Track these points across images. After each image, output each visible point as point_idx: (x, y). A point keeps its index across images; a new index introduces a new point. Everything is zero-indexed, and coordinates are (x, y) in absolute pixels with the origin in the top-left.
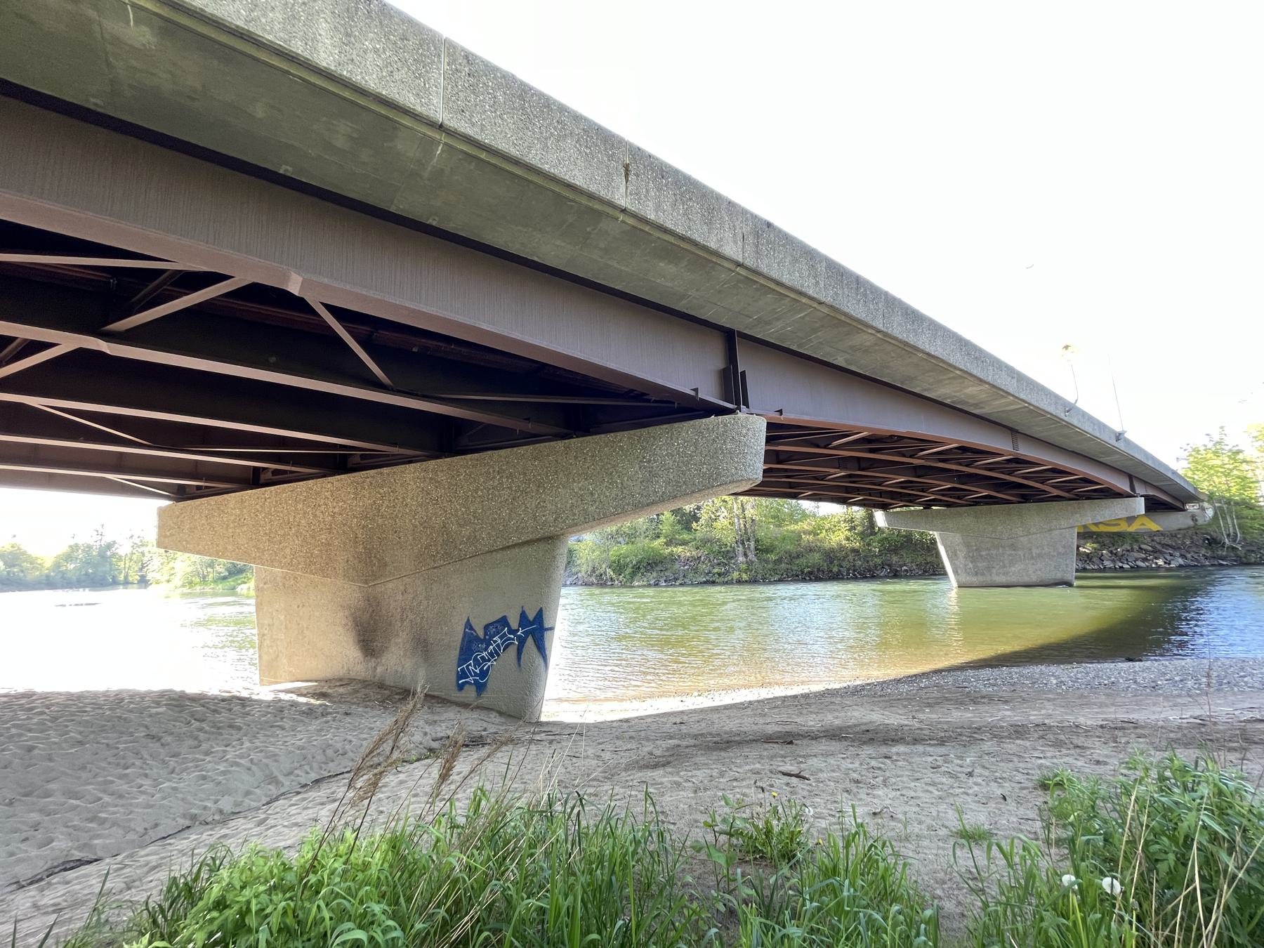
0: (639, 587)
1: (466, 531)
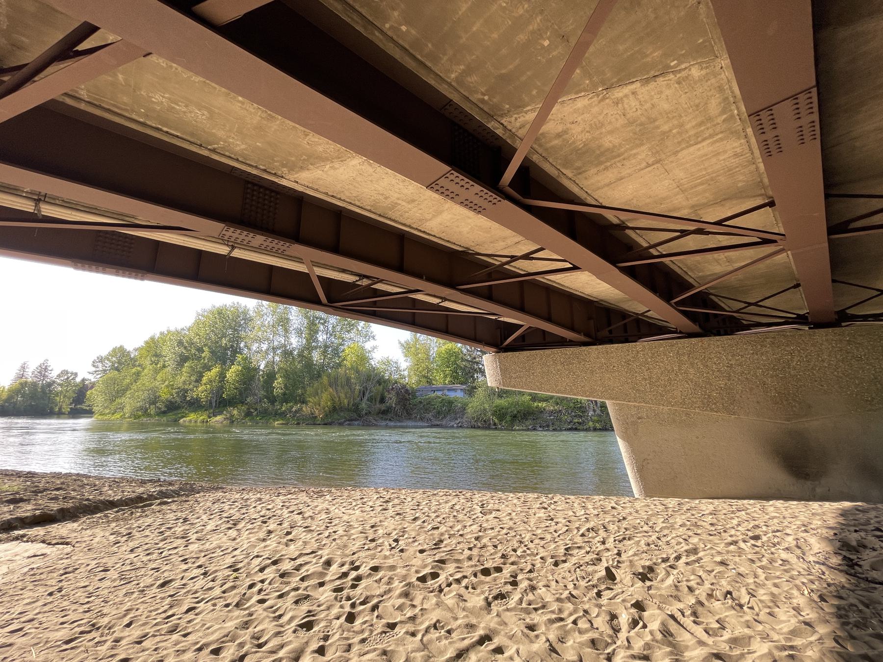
0: (519, 430)
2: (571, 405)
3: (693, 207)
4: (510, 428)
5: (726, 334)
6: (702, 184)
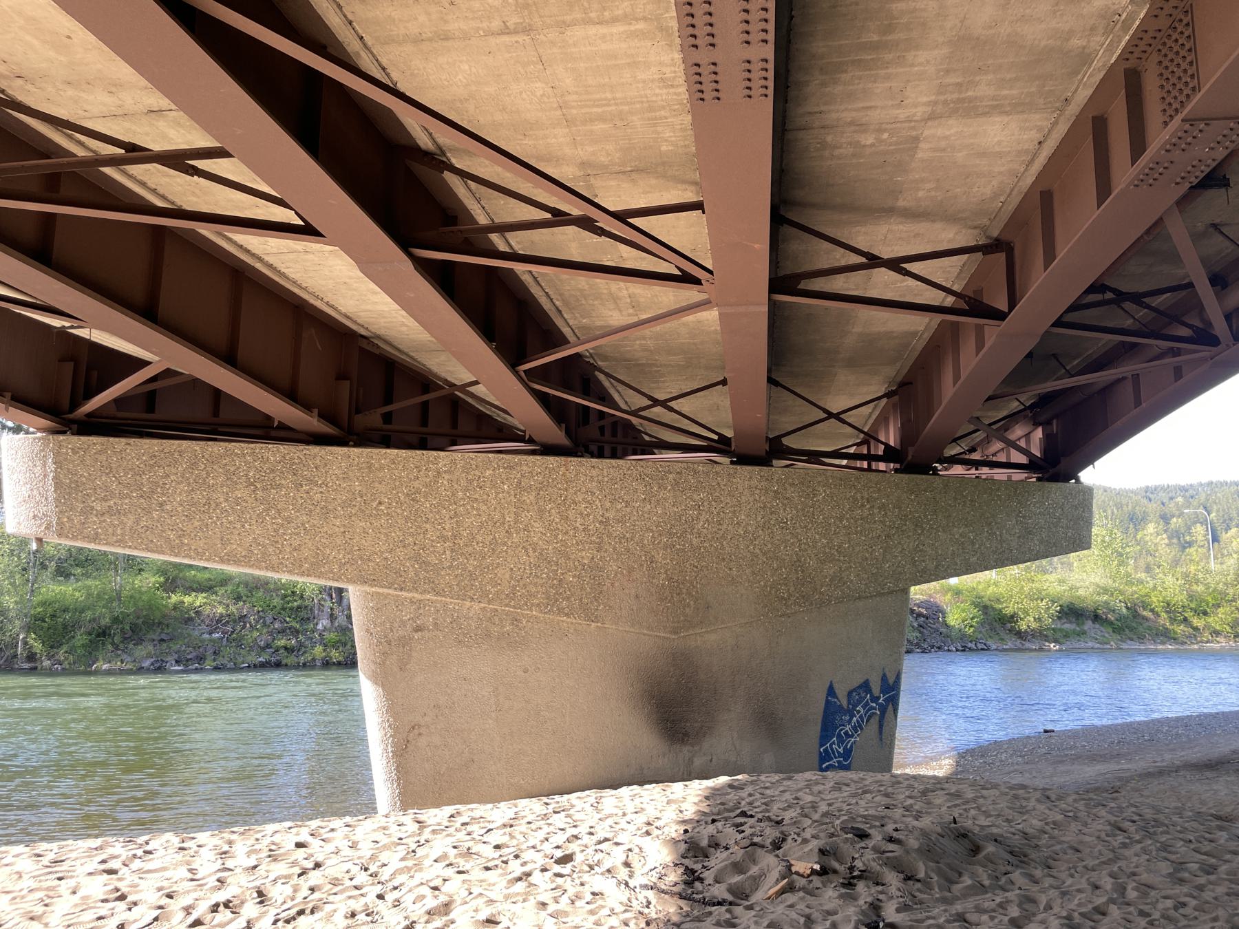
0: (109, 673)
1: (830, 570)
2: (277, 601)
3: (583, 165)
4: (83, 667)
5: (614, 456)
6: (602, 118)
